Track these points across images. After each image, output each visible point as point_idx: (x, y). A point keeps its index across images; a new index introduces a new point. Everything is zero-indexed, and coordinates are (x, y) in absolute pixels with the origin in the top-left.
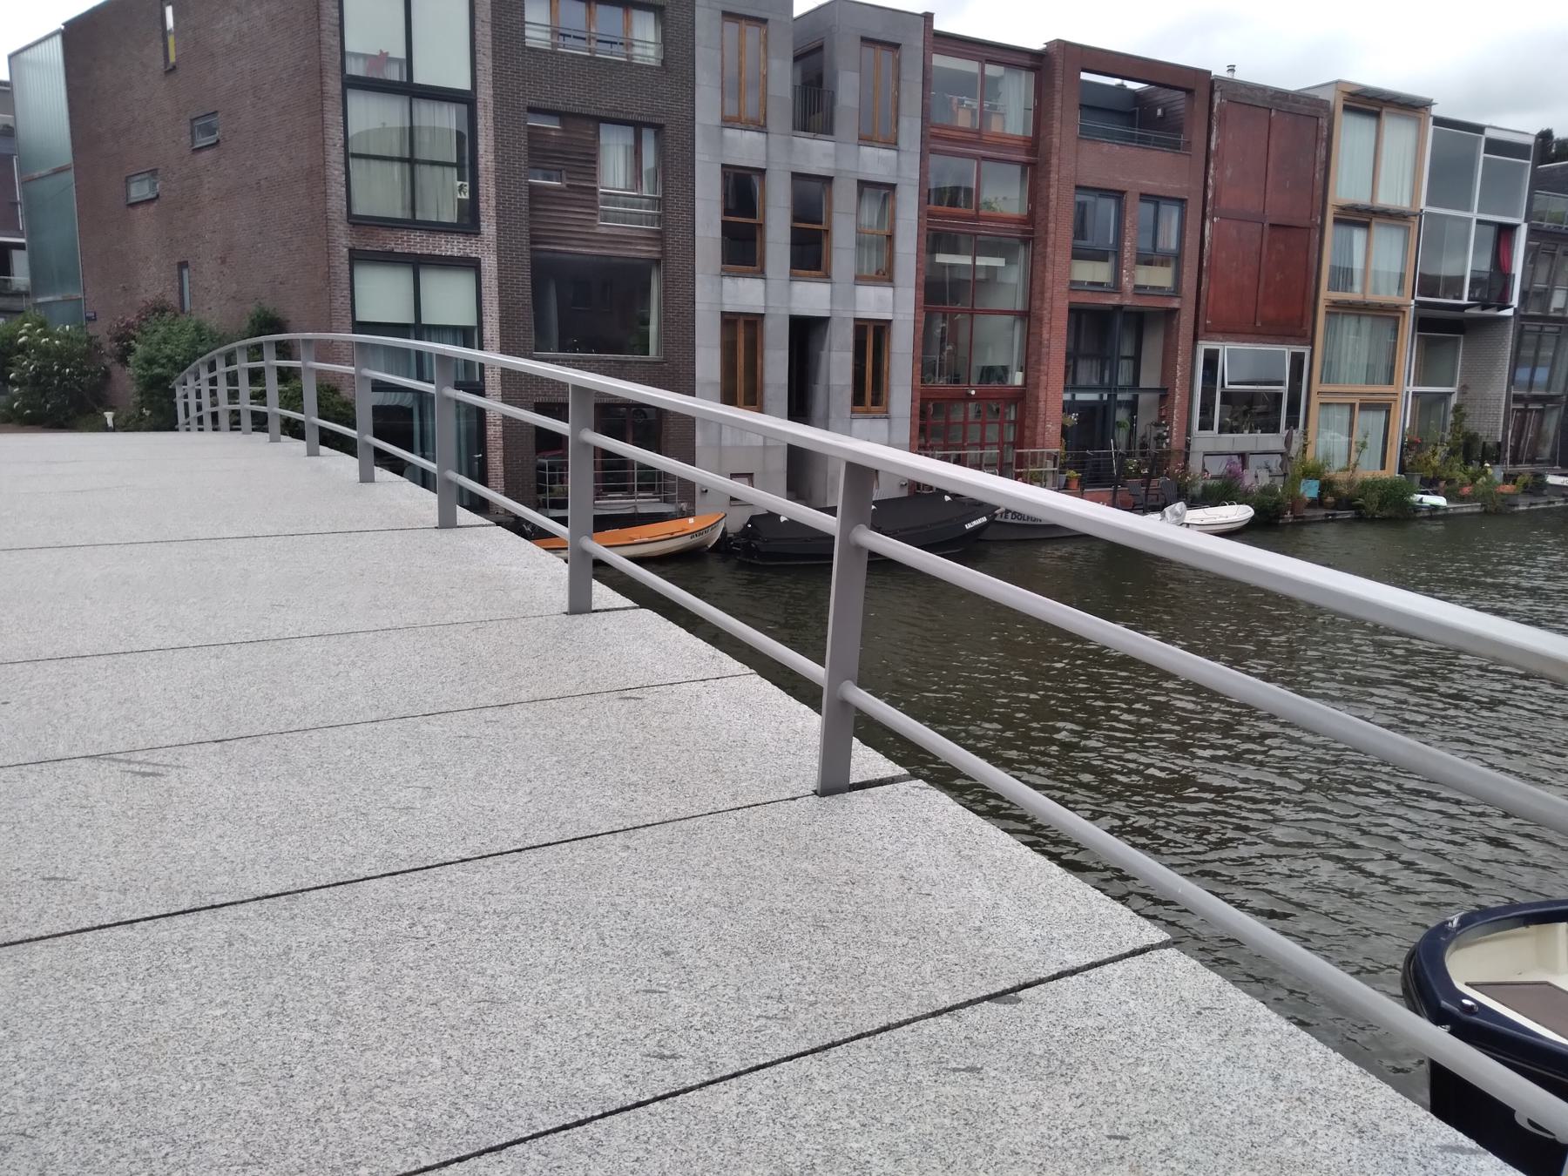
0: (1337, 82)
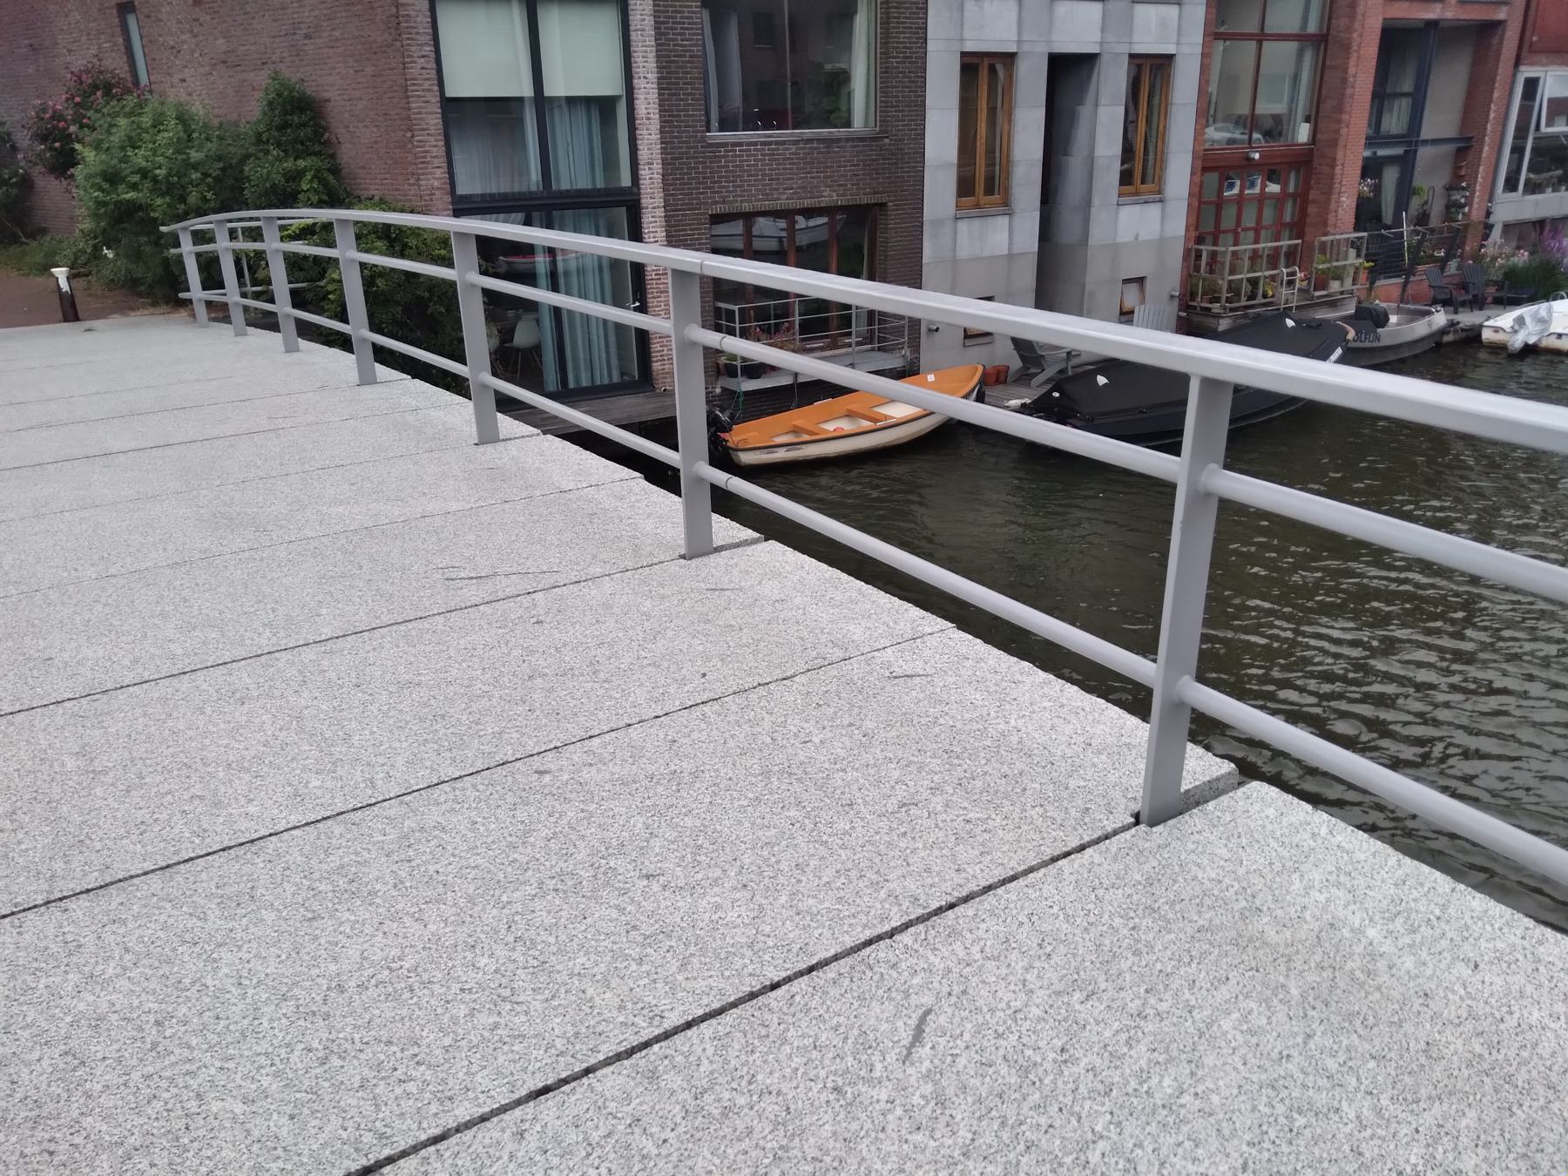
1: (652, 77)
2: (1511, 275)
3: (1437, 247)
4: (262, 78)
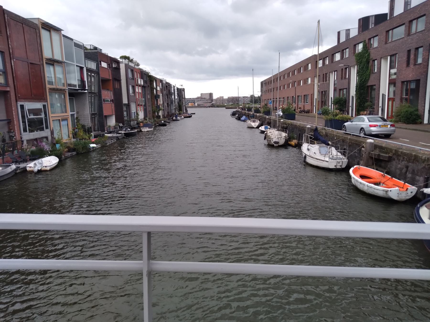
0: (38, 19)
2: (32, 152)
3: (9, 147)
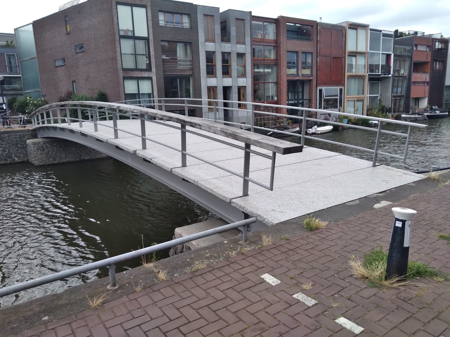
1: (156, 90)
4: (97, 91)
